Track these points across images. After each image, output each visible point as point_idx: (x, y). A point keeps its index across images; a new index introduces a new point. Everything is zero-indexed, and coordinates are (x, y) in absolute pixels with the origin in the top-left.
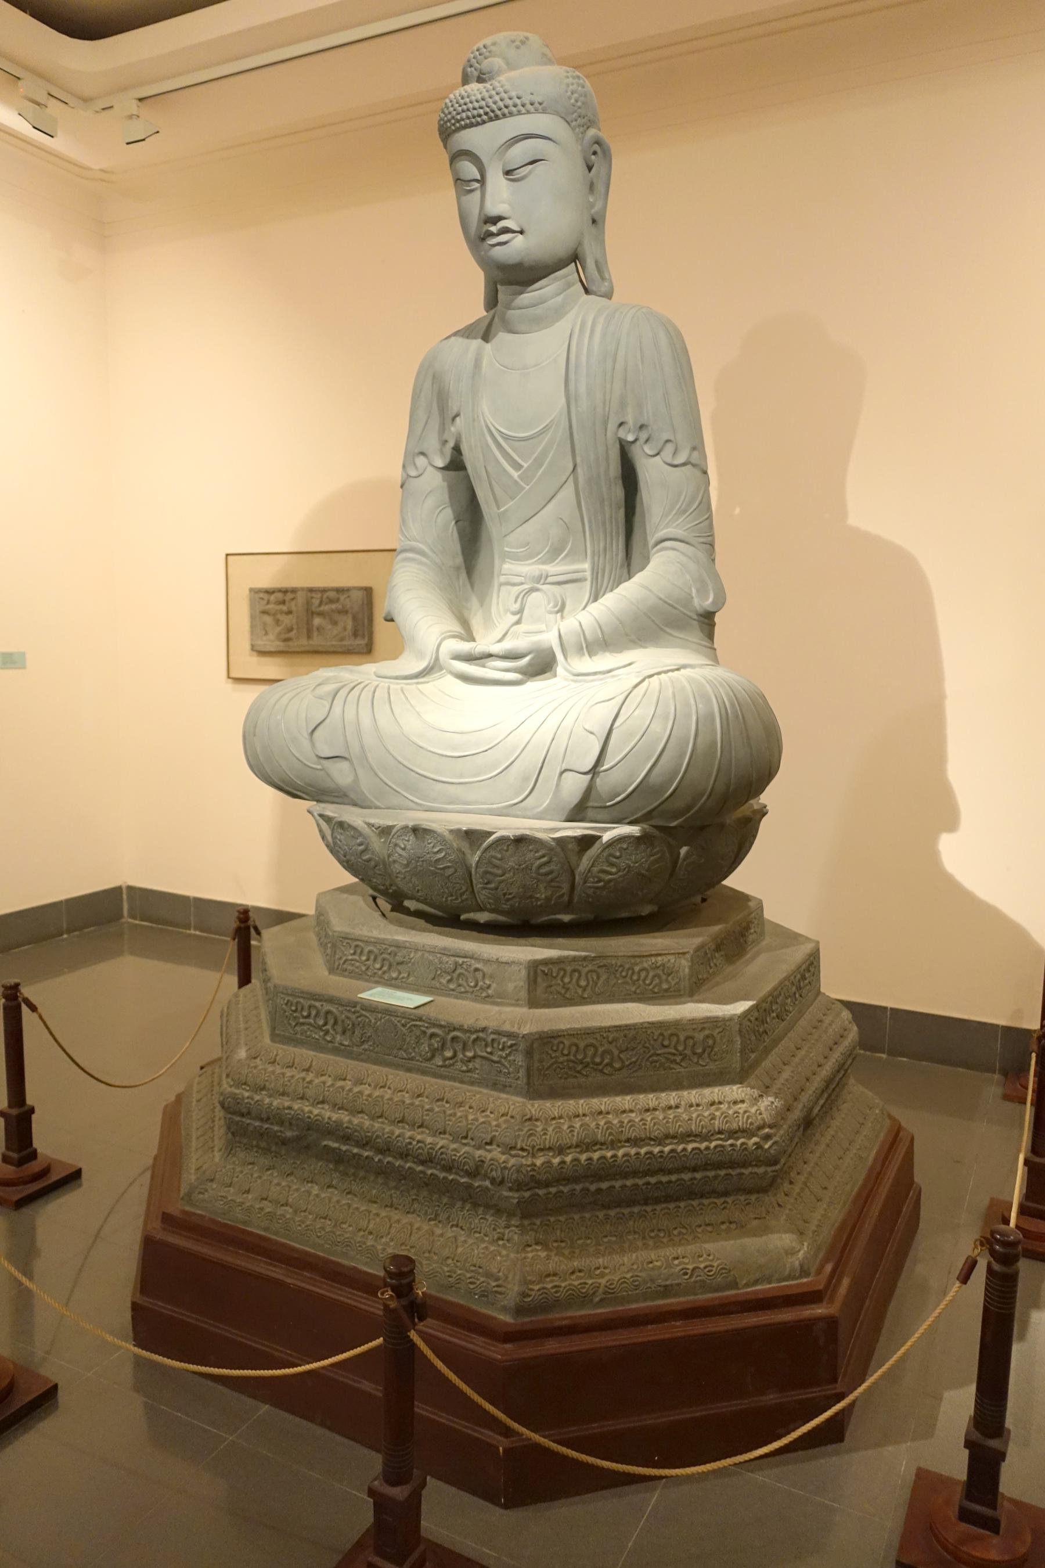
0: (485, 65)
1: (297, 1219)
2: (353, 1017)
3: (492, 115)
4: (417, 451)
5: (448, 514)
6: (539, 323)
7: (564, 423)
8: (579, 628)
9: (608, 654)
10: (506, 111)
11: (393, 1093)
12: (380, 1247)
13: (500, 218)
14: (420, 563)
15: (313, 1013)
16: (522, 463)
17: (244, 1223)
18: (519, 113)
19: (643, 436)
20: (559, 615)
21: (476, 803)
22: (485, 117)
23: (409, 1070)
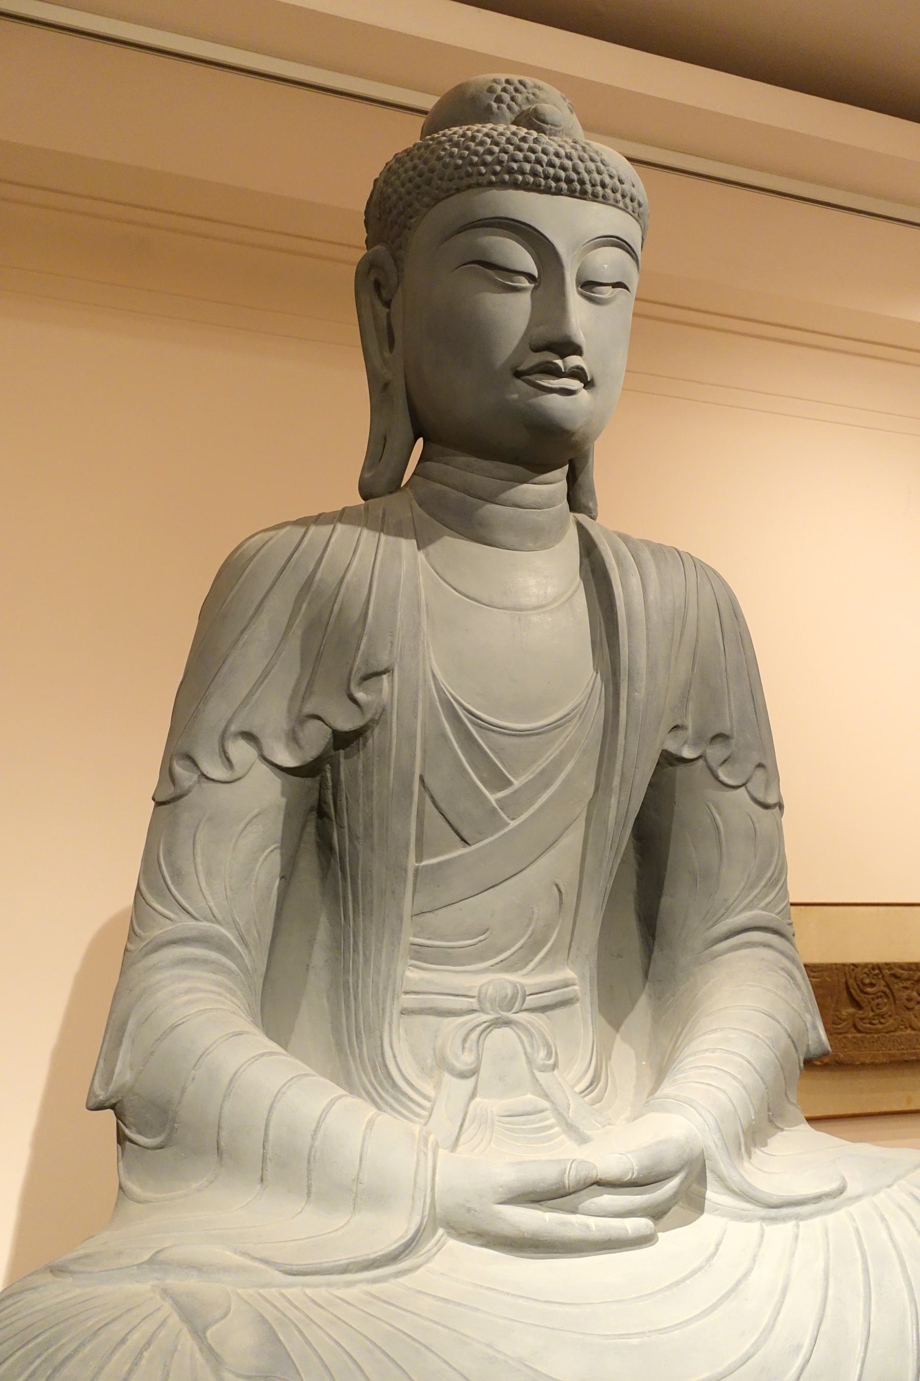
3: (578, 187)
4: (233, 728)
6: (539, 537)
7: (597, 713)
13: (577, 350)
14: (220, 968)
18: (615, 204)
19: (716, 753)
22: (564, 186)
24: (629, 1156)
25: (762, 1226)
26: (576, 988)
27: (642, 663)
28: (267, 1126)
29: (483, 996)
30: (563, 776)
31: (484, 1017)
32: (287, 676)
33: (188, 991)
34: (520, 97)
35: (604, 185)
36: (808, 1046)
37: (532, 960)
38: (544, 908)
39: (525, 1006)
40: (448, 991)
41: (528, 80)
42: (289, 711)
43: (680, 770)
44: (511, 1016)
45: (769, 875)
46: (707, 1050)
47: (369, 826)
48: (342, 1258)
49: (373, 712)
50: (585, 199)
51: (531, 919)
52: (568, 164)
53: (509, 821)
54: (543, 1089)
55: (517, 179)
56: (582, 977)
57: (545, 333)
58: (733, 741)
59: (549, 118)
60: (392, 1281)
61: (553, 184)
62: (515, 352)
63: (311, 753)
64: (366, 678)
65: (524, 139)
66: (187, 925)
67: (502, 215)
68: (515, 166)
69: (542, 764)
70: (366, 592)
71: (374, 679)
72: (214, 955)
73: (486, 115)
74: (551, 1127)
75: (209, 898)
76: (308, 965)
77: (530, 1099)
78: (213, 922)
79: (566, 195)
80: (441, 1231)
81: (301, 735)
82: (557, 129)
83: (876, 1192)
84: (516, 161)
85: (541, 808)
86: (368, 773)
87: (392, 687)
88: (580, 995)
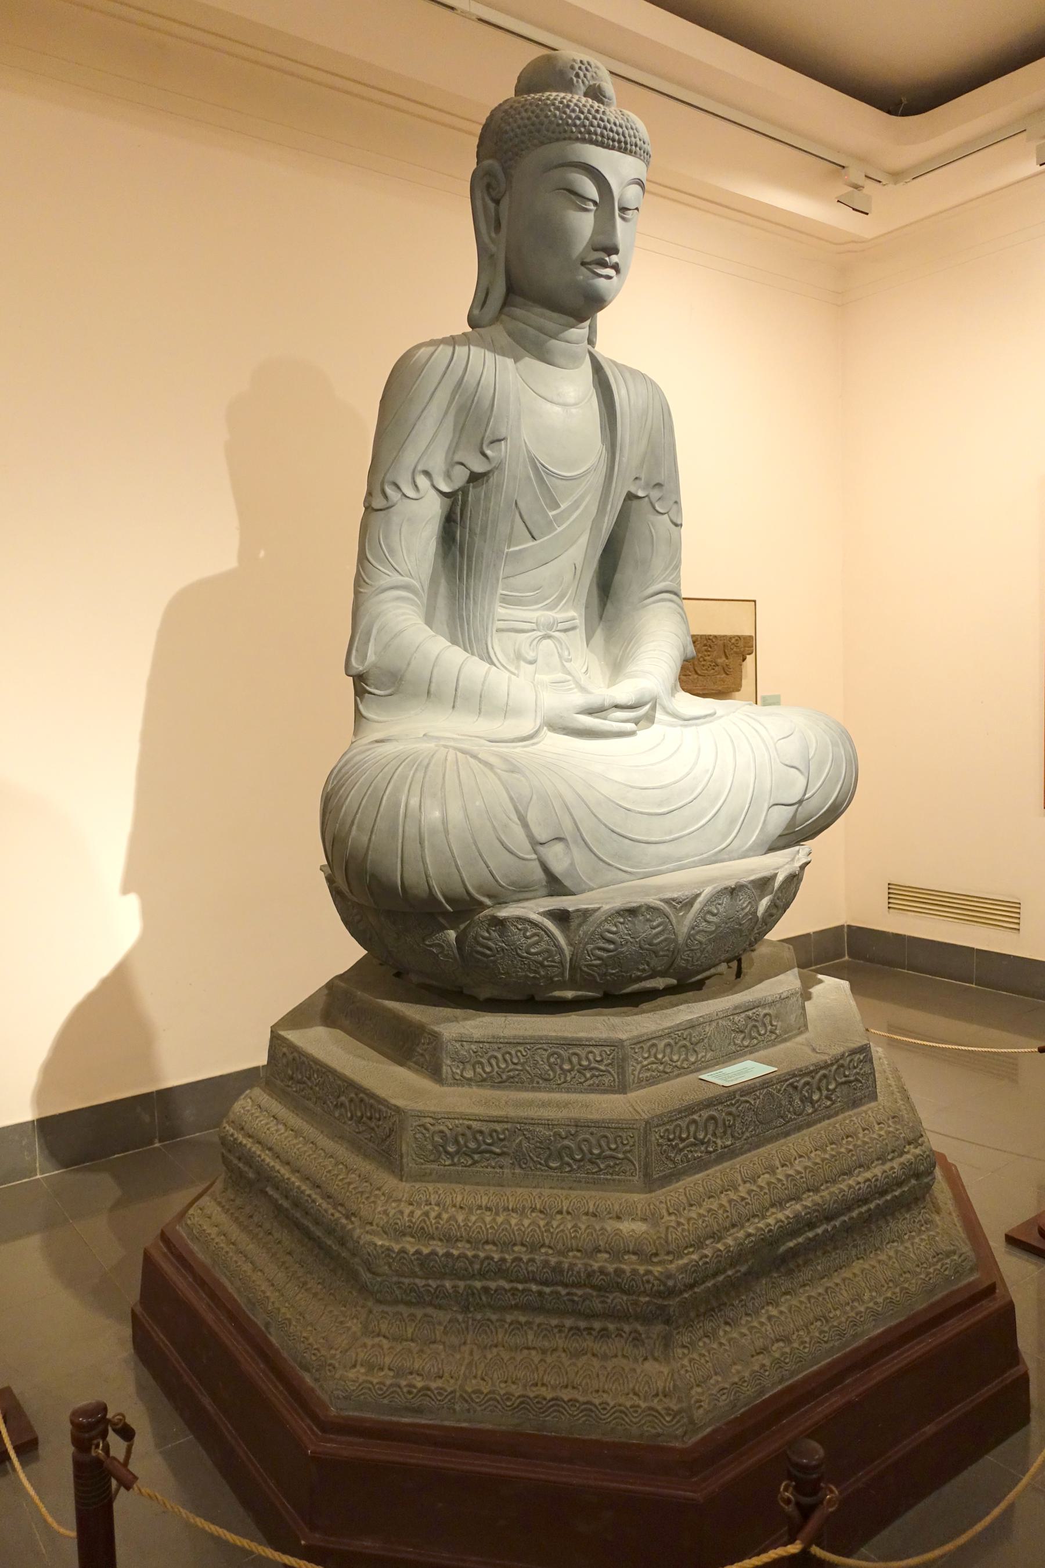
1: (795, 1345)
2: (733, 1109)
4: (420, 468)
6: (574, 361)
7: (603, 470)
11: (809, 1158)
12: (871, 1305)
15: (692, 1128)
17: (762, 1392)
19: (655, 494)
21: (687, 856)
22: (616, 144)
23: (787, 1134)
28: (458, 680)
34: (589, 75)
38: (568, 577)
43: (635, 503)
47: (484, 528)
48: (512, 736)
52: (620, 130)
64: (492, 442)
65: (597, 111)
66: (396, 579)
69: (576, 496)
70: (492, 391)
73: (568, 86)
77: (560, 676)
86: (487, 497)
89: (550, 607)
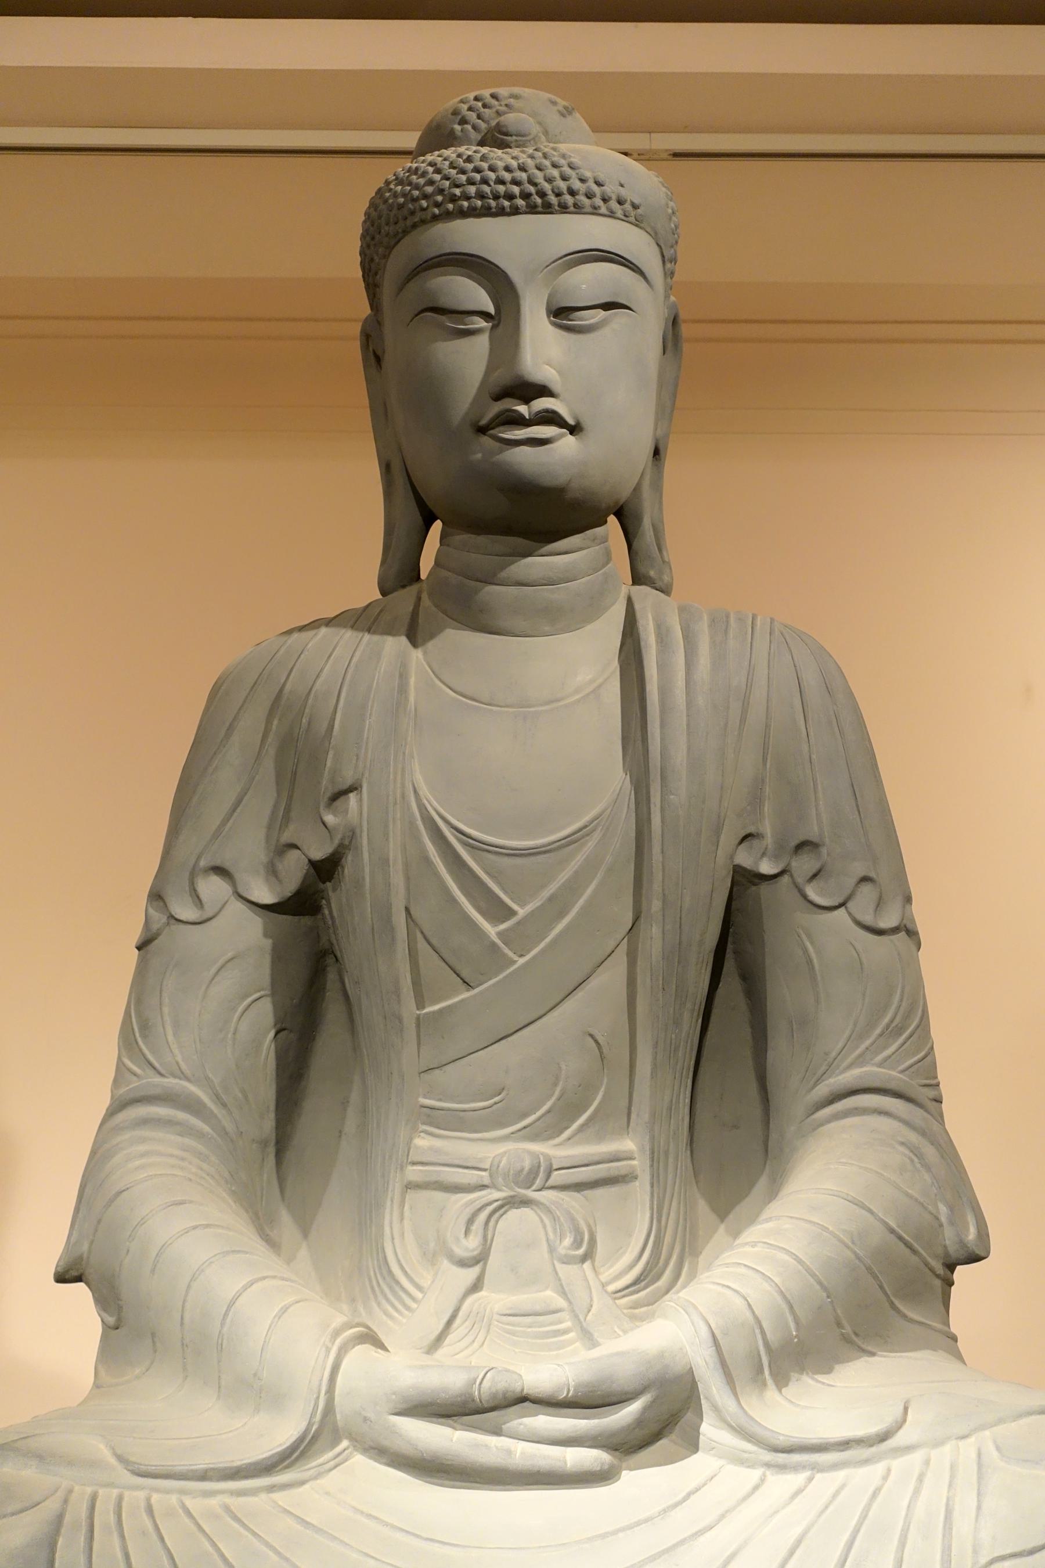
0: (510, 119)
3: (539, 201)
4: (202, 863)
5: (264, 1013)
6: (557, 619)
8: (748, 1314)
9: (806, 1379)
10: (569, 199)
13: (544, 391)
16: (515, 907)
18: (595, 211)
19: (803, 866)
20: (587, 1265)
22: (520, 202)
24: (566, 1367)
25: (764, 1475)
26: (635, 1162)
27: (679, 757)
29: (494, 1168)
30: (581, 902)
31: (496, 1195)
32: (262, 804)
33: (143, 1155)
35: (572, 193)
36: (945, 1247)
37: (567, 1128)
39: (550, 1183)
40: (457, 1162)
41: (503, 92)
42: (267, 841)
43: (764, 889)
44: (530, 1193)
45: (886, 1020)
46: (747, 1244)
48: (202, 1462)
49: (339, 836)
50: (551, 213)
51: (557, 1078)
52: (524, 176)
53: (515, 958)
54: (561, 1285)
55: (461, 206)
56: (642, 1149)
57: (502, 377)
58: (824, 851)
59: (512, 129)
60: (263, 1496)
61: (506, 203)
62: (472, 404)
63: (291, 885)
67: (448, 251)
68: (457, 192)
71: (342, 799)
72: (181, 1115)
74: (565, 1332)
75: (176, 1052)
76: (340, 1132)
77: (550, 1296)
78: (180, 1079)
79: (526, 213)
80: (345, 1443)
81: (280, 867)
82: (528, 138)
83: (938, 1443)
84: (457, 186)
85: (555, 941)
87: (361, 806)
88: (639, 1172)
89: (535, 1134)
